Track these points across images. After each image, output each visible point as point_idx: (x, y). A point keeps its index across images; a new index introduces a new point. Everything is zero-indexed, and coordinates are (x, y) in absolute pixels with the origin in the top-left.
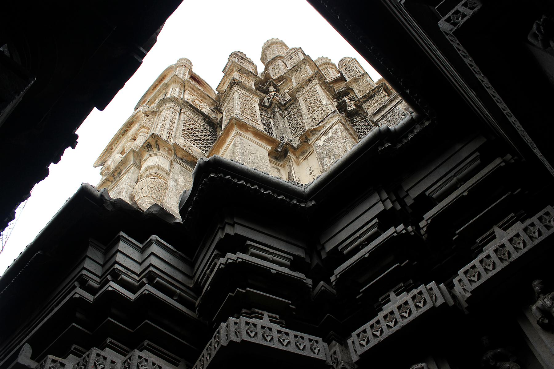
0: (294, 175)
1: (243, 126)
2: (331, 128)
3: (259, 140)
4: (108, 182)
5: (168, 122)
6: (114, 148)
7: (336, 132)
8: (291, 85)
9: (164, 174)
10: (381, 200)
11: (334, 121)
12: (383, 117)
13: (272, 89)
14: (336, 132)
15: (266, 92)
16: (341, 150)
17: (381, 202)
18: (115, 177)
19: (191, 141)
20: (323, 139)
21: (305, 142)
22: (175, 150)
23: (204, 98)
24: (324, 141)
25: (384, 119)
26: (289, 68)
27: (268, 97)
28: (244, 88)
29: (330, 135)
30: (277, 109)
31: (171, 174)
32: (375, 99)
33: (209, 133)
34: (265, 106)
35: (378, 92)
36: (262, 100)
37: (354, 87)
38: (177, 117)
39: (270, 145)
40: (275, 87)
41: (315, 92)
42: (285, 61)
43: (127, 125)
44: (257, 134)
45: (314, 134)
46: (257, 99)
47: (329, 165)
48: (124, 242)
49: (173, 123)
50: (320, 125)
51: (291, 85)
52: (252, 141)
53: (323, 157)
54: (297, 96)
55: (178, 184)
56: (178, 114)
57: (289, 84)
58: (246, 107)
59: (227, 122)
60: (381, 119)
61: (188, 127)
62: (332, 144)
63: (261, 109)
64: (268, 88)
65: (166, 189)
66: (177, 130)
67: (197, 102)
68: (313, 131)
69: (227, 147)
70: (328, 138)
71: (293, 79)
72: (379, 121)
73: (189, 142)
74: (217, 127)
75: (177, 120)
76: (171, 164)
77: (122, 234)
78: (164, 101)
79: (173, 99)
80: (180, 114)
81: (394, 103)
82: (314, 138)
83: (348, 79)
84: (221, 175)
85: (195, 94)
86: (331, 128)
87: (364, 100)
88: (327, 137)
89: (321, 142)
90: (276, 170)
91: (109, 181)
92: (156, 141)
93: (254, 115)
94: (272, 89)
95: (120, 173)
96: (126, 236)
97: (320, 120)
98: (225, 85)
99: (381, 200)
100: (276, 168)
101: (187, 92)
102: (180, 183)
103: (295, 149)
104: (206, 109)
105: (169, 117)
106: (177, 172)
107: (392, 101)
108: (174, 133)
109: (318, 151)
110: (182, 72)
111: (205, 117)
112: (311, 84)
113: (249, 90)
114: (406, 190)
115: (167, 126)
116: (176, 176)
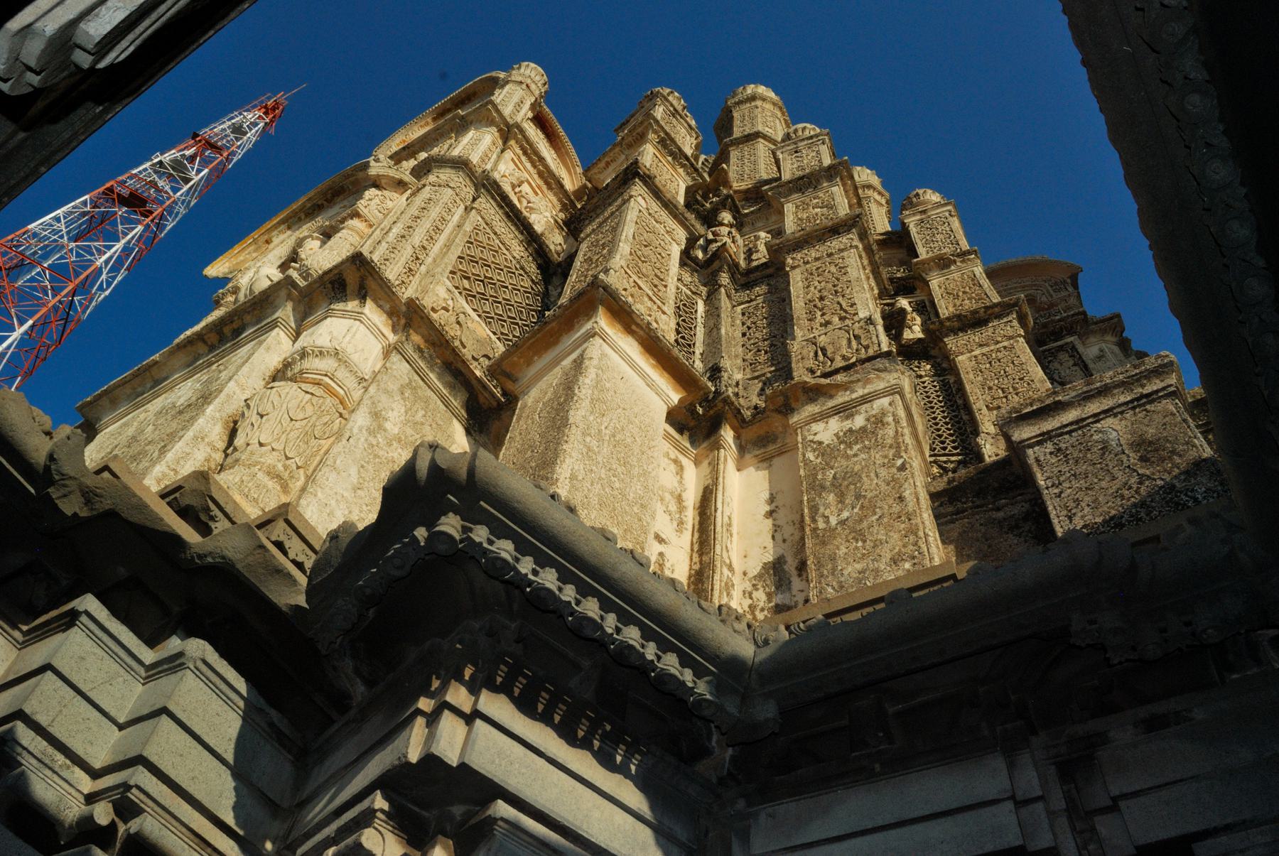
0: (719, 505)
1: (625, 317)
2: (866, 399)
3: (653, 367)
4: (200, 344)
5: (425, 225)
6: (276, 241)
7: (879, 421)
8: (775, 222)
9: (351, 382)
10: (1013, 798)
11: (881, 385)
12: (1046, 437)
13: (726, 217)
14: (879, 421)
15: (710, 220)
16: (883, 487)
17: (1009, 805)
18: (222, 340)
19: (469, 296)
20: (835, 425)
21: (780, 412)
22: (409, 317)
23: (547, 183)
24: (836, 435)
25: (1049, 447)
26: (786, 176)
27: (710, 236)
28: (657, 193)
29: (859, 421)
30: (724, 278)
31: (372, 390)
32: (987, 332)
33: (527, 283)
34: (695, 260)
35: (999, 317)
36: (692, 241)
37: (936, 282)
38: (456, 218)
39: (677, 392)
40: (735, 211)
41: (843, 269)
42: (778, 153)
43: (325, 194)
44: (652, 345)
45: (812, 401)
46: (682, 235)
47: (833, 521)
48: (91, 635)
49: (438, 230)
50: (840, 378)
51: (775, 222)
52: (633, 365)
53: (823, 487)
54: (789, 261)
55: (380, 427)
56: (461, 209)
57: (774, 218)
58: (647, 251)
59: (579, 287)
60: (1039, 443)
61: (476, 252)
62: (858, 458)
63: (683, 264)
64: (715, 211)
65: (339, 435)
66: (448, 246)
67: (525, 188)
68: (813, 393)
69: (556, 362)
70: (850, 430)
71: (789, 208)
72: (1031, 446)
73: (462, 301)
74: (555, 274)
75: (451, 226)
76: (387, 354)
77: (89, 603)
78: (442, 162)
79: (461, 165)
80: (468, 210)
81: (1094, 407)
82: (811, 409)
83: (923, 253)
84: (480, 534)
85: (528, 165)
86: (866, 399)
87: (956, 324)
88: (847, 424)
89: (827, 431)
90: (673, 467)
91: (204, 342)
92: (363, 279)
93: (659, 281)
94: (726, 217)
95: (237, 332)
96: (102, 613)
97: (839, 363)
98: (611, 168)
99: (1013, 798)
100: (676, 461)
101: (508, 155)
102: (388, 425)
103: (744, 420)
104: (544, 214)
105: (434, 212)
106: (393, 386)
107: (1087, 397)
108: (429, 260)
109: (811, 456)
110: (516, 99)
111: (532, 239)
112: (835, 244)
113: (668, 205)
114: (1115, 791)
115: (418, 238)
116: (384, 398)
